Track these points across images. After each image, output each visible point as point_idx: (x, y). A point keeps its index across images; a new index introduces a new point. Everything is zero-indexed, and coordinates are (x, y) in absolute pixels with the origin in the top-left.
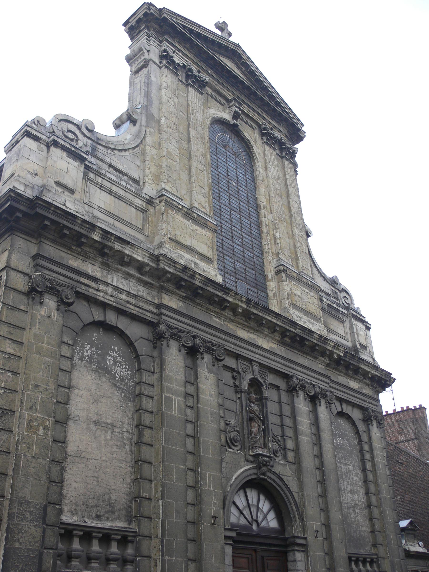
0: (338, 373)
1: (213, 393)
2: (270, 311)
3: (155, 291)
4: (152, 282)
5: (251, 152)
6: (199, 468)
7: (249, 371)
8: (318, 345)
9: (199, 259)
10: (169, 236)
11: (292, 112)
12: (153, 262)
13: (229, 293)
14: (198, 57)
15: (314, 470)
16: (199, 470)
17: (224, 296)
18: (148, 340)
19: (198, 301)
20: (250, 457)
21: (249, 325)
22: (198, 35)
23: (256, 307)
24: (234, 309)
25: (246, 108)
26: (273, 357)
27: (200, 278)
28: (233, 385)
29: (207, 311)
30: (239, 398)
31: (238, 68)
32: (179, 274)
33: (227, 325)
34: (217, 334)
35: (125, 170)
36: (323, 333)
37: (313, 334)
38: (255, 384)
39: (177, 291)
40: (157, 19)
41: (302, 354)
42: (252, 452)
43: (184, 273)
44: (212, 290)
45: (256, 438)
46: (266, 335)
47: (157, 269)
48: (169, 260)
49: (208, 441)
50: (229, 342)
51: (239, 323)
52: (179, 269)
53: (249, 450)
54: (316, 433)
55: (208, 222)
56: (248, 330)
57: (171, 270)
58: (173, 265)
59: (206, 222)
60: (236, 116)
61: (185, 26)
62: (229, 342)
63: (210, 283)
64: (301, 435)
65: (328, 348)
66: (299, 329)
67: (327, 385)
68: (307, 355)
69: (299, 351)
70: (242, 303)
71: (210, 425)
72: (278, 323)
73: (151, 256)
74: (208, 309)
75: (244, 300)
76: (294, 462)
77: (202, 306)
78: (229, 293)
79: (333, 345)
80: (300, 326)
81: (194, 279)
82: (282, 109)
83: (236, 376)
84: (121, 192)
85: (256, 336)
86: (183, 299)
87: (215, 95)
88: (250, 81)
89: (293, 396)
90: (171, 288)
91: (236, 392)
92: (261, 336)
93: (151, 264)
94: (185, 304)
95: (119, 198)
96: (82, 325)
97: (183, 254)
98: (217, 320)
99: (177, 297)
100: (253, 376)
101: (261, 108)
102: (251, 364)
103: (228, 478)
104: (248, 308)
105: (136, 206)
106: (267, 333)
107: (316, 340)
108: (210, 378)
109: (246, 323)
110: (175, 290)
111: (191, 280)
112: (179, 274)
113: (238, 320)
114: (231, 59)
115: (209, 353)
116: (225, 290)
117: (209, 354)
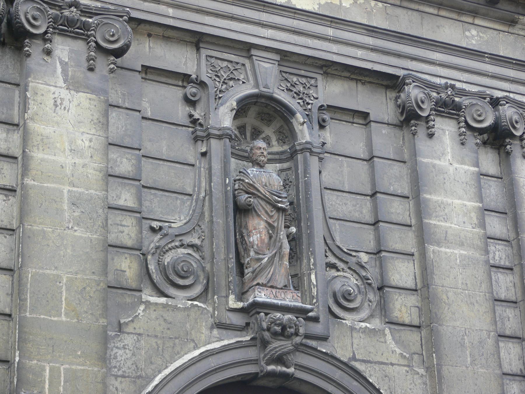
6: (17, 354)
7: (242, 77)
15: (490, 342)
16: (17, 359)
20: (230, 315)
26: (330, 32)
28: (186, 121)
30: (204, 154)
38: (263, 113)
45: (259, 260)
49: (59, 276)
53: (227, 297)
54: (512, 236)
64: (438, 244)
71: (69, 232)
76: (416, 322)
83: (194, 95)
89: (508, 154)
91: (196, 139)
100: (255, 91)
102: (250, 57)
103: (139, 377)
108: (75, 102)
115: (450, 116)
117: (76, 38)
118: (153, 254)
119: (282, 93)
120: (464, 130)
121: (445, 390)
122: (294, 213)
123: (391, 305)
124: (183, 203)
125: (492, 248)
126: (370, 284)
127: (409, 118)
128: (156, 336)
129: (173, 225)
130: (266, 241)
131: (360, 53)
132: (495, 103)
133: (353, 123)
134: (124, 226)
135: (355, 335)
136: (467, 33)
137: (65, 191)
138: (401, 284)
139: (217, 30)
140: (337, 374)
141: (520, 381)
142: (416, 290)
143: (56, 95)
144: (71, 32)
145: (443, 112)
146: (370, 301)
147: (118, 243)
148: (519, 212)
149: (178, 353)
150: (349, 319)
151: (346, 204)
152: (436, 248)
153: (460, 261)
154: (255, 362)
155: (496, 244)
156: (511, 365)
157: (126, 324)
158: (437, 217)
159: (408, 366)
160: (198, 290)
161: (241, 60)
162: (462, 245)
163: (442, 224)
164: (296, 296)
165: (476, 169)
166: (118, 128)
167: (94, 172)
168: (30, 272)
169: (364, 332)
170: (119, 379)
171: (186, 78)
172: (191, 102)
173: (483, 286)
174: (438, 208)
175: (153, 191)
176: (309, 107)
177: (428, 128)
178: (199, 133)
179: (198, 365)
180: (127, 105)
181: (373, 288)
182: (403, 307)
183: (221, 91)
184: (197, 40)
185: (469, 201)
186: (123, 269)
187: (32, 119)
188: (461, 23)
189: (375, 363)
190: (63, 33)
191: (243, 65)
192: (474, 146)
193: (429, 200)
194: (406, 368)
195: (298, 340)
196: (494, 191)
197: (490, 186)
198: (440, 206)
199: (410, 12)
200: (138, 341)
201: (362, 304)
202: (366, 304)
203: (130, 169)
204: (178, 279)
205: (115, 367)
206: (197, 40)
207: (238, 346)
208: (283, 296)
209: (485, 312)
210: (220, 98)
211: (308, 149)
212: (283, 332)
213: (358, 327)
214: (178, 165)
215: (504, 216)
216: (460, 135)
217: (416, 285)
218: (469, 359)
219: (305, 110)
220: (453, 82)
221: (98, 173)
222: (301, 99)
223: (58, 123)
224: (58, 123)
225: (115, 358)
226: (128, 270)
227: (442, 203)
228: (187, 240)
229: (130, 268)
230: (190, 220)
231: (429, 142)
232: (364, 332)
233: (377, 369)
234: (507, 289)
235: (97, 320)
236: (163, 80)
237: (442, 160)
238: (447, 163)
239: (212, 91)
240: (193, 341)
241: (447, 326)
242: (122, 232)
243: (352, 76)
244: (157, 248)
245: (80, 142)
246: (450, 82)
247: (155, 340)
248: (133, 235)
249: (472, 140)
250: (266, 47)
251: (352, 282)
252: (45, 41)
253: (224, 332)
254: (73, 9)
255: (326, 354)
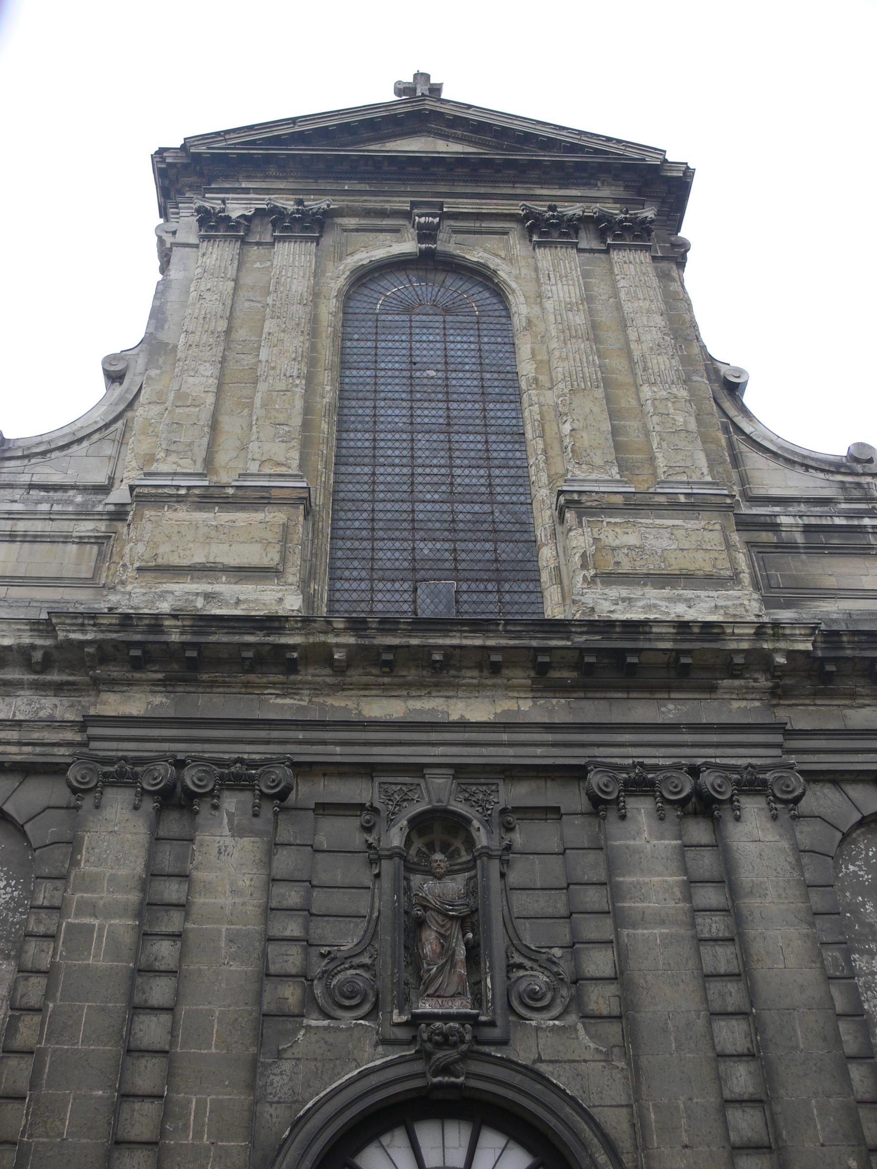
0: (847, 702)
1: (244, 882)
2: (438, 623)
3: (89, 696)
4: (71, 678)
5: (497, 285)
8: (688, 652)
9: (232, 581)
10: (137, 564)
11: (619, 141)
12: (46, 637)
13: (284, 628)
14: (306, 178)
15: (701, 1022)
17: (271, 639)
18: (582, 814)
19: (205, 677)
20: (395, 1030)
21: (402, 680)
22: (277, 141)
23: (390, 630)
24: (321, 656)
25: (467, 204)
26: (505, 737)
27: (179, 623)
28: (364, 847)
29: (249, 690)
31: (446, 137)
32: (114, 636)
33: (324, 704)
34: (275, 734)
35: (68, 480)
36: (741, 611)
37: (647, 629)
39: (137, 675)
40: (185, 166)
41: (648, 695)
42: (401, 1013)
43: (129, 629)
44: (225, 639)
46: (479, 688)
47: (59, 647)
48: (76, 618)
50: (324, 743)
51: (366, 687)
52: (110, 625)
55: (273, 490)
56: (405, 693)
57: (89, 637)
58: (92, 622)
59: (266, 495)
60: (426, 234)
61: (253, 142)
62: (324, 743)
63: (214, 624)
64: (634, 927)
65: (733, 646)
66: (582, 633)
67: (777, 752)
68: (669, 692)
69: (627, 689)
70: (337, 635)
72: (491, 643)
73: (36, 627)
74: (247, 684)
75: (341, 626)
77: (225, 684)
78: (284, 628)
79: (752, 631)
80: (580, 626)
81: (163, 632)
82: (588, 153)
83: (368, 822)
84: (38, 527)
85: (441, 701)
86: (165, 686)
87: (369, 222)
88: (484, 145)
90: (116, 674)
92: (460, 694)
93: (39, 642)
94: (173, 695)
95: (35, 539)
96: (839, 836)
97: (217, 588)
98: (288, 701)
99: (148, 688)
100: (429, 806)
101: (520, 182)
102: (423, 777)
103: (295, 1102)
104: (366, 642)
105: (80, 537)
106: (475, 681)
107: (668, 640)
109: (386, 680)
110: (129, 675)
111: (151, 638)
112: (114, 636)
113: (356, 679)
114: (420, 132)
116: (267, 624)
118: (320, 979)
119: (460, 805)
120: (660, 804)
121: (644, 1082)
122: (470, 919)
123: (586, 999)
124: (357, 925)
125: (699, 920)
126: (562, 980)
127: (599, 806)
128: (316, 1059)
129: (342, 948)
130: (438, 950)
131: (539, 751)
132: (694, 771)
133: (546, 819)
134: (289, 955)
135: (540, 1034)
136: (663, 709)
137: (224, 930)
138: (598, 974)
139: (386, 757)
140: (517, 1079)
141: (748, 1062)
142: (616, 979)
143: (221, 844)
144: (237, 785)
145: (636, 791)
146: (563, 997)
147: (283, 972)
148: (733, 878)
149: (339, 1074)
150: (536, 1020)
151: (537, 901)
152: (631, 931)
153: (661, 941)
154: (423, 1075)
155: (712, 916)
156: (735, 1044)
157: (285, 1050)
158: (631, 899)
159: (605, 1061)
160: (366, 1008)
161: (416, 781)
162: (663, 923)
163: (638, 905)
164: (465, 1003)
165: (679, 842)
166: (288, 864)
167: (253, 908)
168: (183, 1010)
169: (552, 1030)
170: (274, 1106)
171: (361, 807)
172: (368, 829)
173: (690, 963)
174: (633, 890)
175: (326, 919)
176: (489, 812)
177: (619, 810)
178: (372, 857)
179: (357, 1084)
180: (298, 842)
181: (566, 983)
182: (600, 999)
183: (393, 814)
184: (368, 770)
185: (671, 876)
186: (286, 996)
187: (196, 868)
188: (655, 701)
189: (565, 1062)
190: (230, 788)
191: (419, 785)
192: (675, 819)
193: (622, 882)
194: (602, 1063)
195: (464, 1047)
196: (706, 863)
197: (703, 857)
198: (635, 887)
199: (596, 702)
200: (296, 1065)
201: (553, 1000)
202: (558, 1001)
203: (298, 900)
204: (343, 1000)
205: (271, 1094)
206: (368, 770)
207: (402, 1061)
208: (450, 1004)
209: (693, 991)
210: (392, 820)
211: (487, 853)
212: (445, 1041)
213: (544, 1026)
214: (353, 890)
215: (722, 885)
216: (658, 811)
217: (616, 973)
218: (673, 1045)
219: (485, 816)
220: (641, 760)
221: (257, 909)
222: (481, 806)
223: (220, 869)
224: (220, 869)
225: (272, 1084)
226: (291, 998)
227: (638, 883)
228: (356, 961)
229: (293, 995)
230: (361, 941)
231: (622, 824)
232: (552, 1030)
233: (567, 1068)
234: (728, 962)
235: (247, 1048)
236: (341, 813)
237: (637, 839)
238: (643, 842)
239: (384, 814)
240: (355, 1060)
241: (646, 1012)
242: (287, 961)
243: (540, 775)
244: (324, 972)
245: (241, 882)
246: (636, 760)
247: (314, 1063)
248: (298, 963)
249: (672, 814)
250: (438, 764)
251: (540, 980)
252: (213, 797)
253: (390, 1048)
254: (238, 765)
255: (501, 1058)
